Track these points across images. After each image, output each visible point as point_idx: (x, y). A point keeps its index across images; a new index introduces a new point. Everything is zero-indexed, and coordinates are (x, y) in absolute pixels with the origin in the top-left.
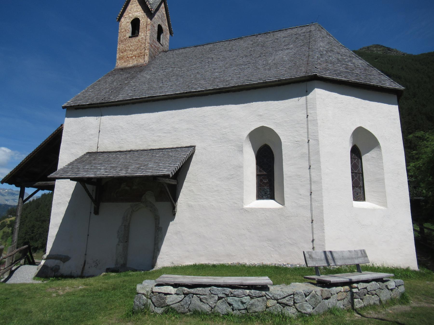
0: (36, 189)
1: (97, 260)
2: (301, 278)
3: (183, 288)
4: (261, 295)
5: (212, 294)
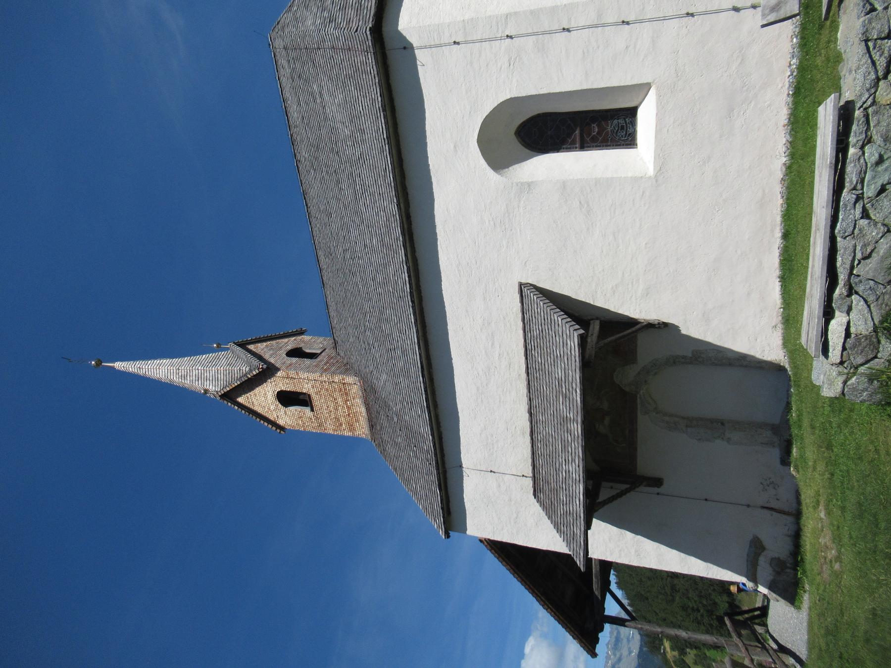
0: (608, 596)
1: (761, 483)
2: (825, 32)
3: (834, 298)
4: (863, 119)
5: (853, 233)
